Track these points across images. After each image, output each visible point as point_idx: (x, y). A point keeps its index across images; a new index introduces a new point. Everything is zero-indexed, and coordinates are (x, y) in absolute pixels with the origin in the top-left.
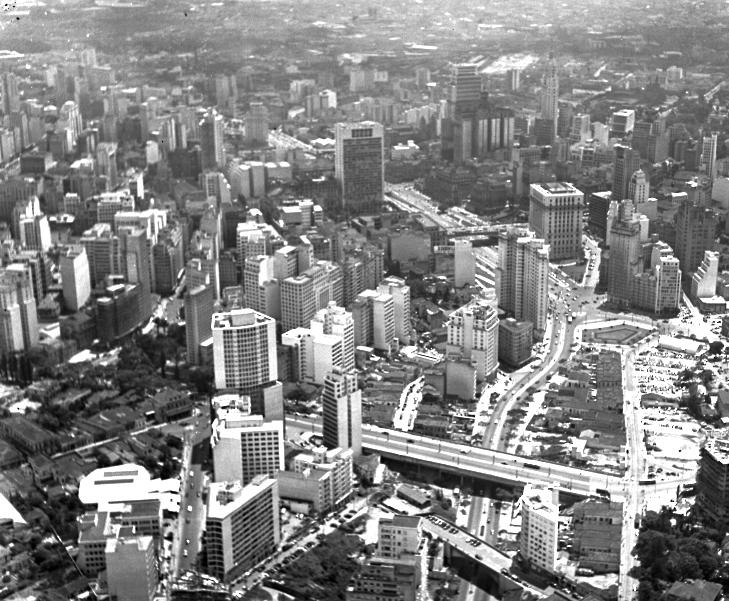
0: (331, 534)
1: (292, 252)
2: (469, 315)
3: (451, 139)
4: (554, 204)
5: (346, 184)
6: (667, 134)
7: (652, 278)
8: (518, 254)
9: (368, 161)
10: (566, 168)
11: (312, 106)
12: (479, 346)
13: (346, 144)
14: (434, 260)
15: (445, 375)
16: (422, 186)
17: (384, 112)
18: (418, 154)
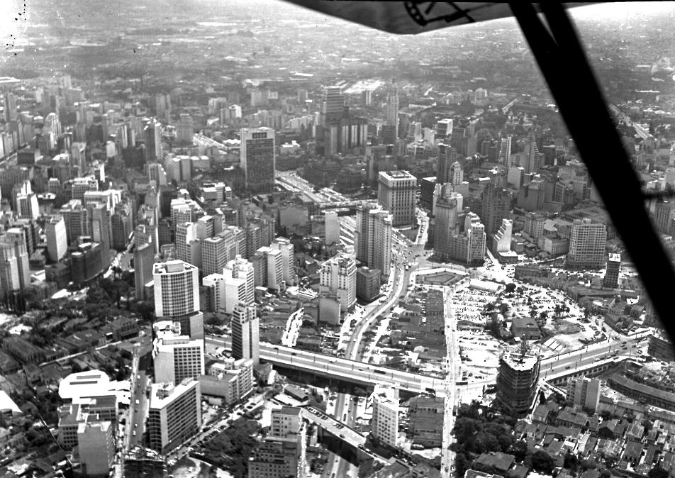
1: (210, 220)
2: (335, 264)
3: (322, 140)
5: (248, 172)
7: (465, 238)
8: (370, 221)
9: (264, 155)
11: (224, 116)
12: (342, 287)
14: (311, 225)
15: (318, 307)
16: (302, 173)
18: (300, 150)
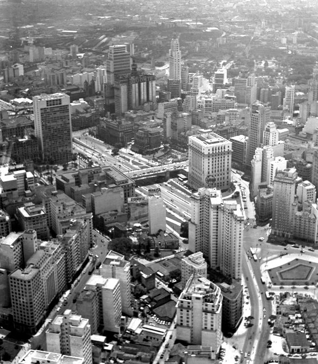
0: (25, 343)
1: (18, 240)
2: (198, 298)
3: (112, 97)
4: (211, 152)
5: (44, 141)
8: (212, 213)
11: (8, 75)
12: (209, 327)
13: (43, 111)
16: (95, 133)
17: (58, 77)
18: (88, 108)
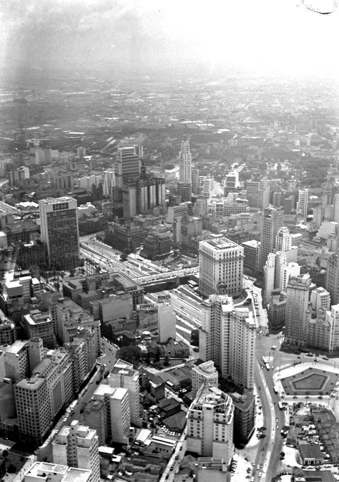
0: (31, 455)
1: (23, 349)
3: (121, 201)
4: (222, 258)
6: (269, 188)
8: (224, 321)
9: (67, 227)
10: (208, 220)
11: (14, 178)
12: (220, 438)
13: (49, 216)
16: (103, 238)
17: (64, 181)
